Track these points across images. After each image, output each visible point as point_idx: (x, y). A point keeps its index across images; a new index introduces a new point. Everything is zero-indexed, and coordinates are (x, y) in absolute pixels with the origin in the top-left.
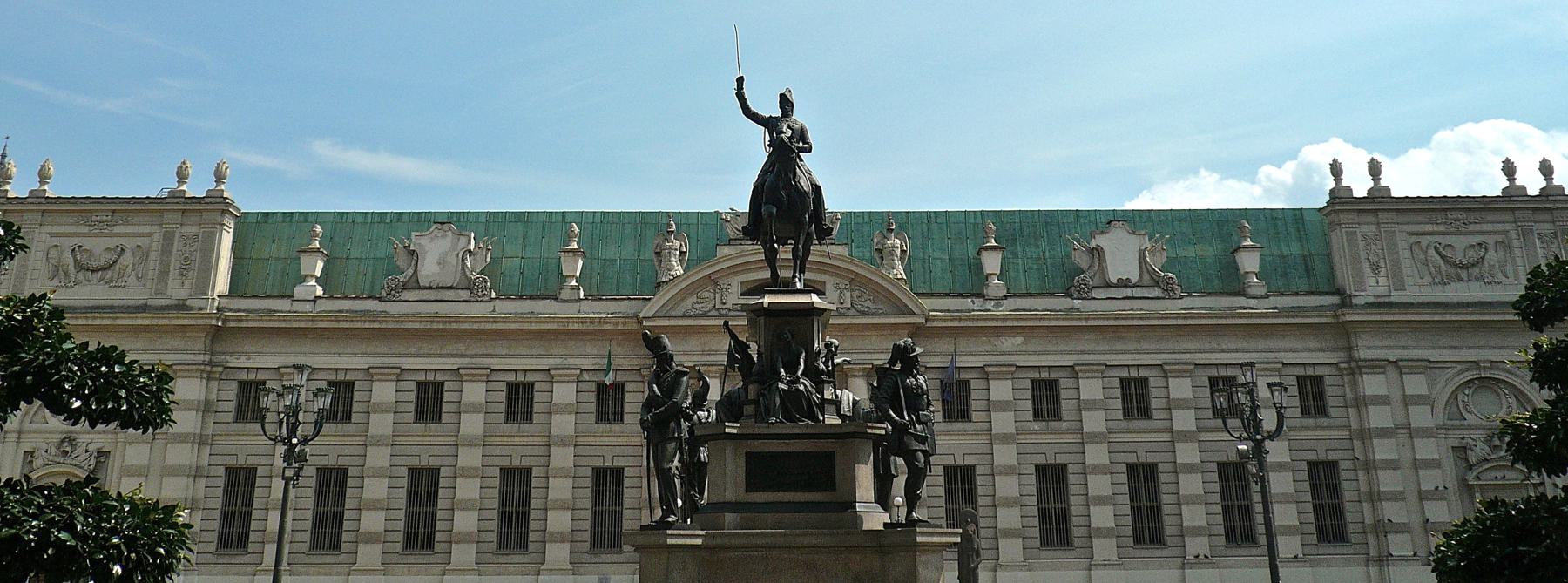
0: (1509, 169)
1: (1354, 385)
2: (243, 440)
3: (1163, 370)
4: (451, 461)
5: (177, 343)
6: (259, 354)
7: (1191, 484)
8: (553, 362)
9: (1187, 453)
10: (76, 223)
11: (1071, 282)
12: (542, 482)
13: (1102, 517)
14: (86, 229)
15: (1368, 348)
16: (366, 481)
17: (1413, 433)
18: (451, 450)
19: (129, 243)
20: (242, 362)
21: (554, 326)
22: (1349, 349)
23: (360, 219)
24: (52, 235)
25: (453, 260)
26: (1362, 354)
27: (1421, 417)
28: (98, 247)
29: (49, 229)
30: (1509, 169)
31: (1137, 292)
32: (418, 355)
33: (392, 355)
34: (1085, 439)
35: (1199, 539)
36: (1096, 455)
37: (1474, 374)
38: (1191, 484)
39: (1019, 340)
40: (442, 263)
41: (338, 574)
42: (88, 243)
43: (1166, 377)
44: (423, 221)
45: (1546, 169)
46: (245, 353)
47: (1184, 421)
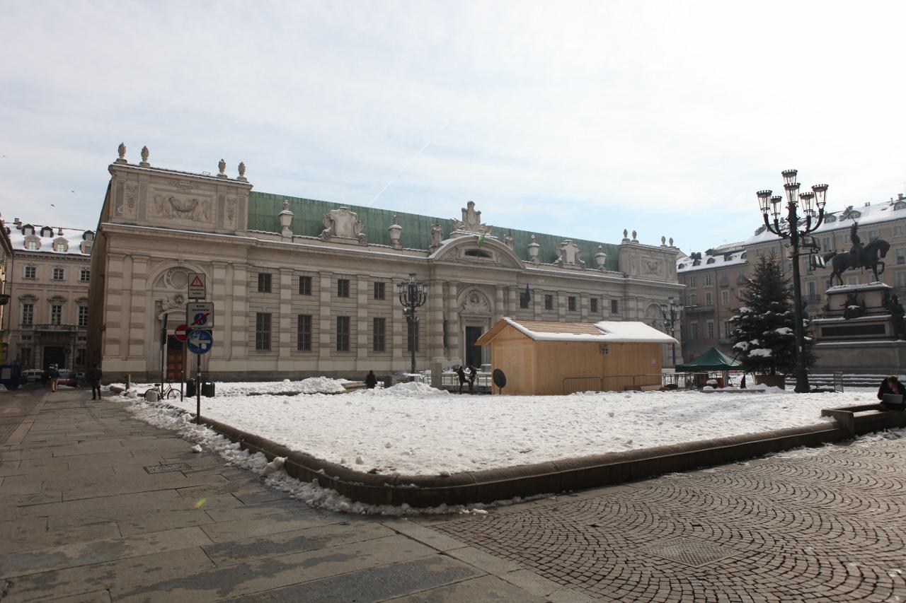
0: (222, 165)
1: (625, 304)
2: (264, 300)
3: (557, 293)
4: (277, 311)
5: (232, 252)
6: (269, 261)
7: (285, 323)
8: (394, 275)
9: (285, 309)
10: (170, 184)
11: (317, 230)
12: (390, 324)
13: (362, 339)
14: (175, 189)
15: (631, 293)
16: (321, 321)
17: (131, 293)
18: (355, 310)
19: (201, 199)
20: (261, 264)
21: (396, 260)
22: (625, 292)
23: (295, 201)
24: (156, 189)
25: (350, 226)
26: (631, 294)
27: (139, 285)
28: (183, 199)
29: (155, 186)
30: (222, 165)
31: (351, 242)
32: (343, 268)
33: (329, 267)
34: (281, 302)
35: (364, 349)
36: (325, 311)
37: (176, 264)
38: (325, 325)
39: (543, 281)
40: (345, 227)
41: (313, 361)
42: (176, 196)
43: (280, 274)
44: (337, 206)
45: (242, 168)
46: (261, 260)
47: (363, 299)
